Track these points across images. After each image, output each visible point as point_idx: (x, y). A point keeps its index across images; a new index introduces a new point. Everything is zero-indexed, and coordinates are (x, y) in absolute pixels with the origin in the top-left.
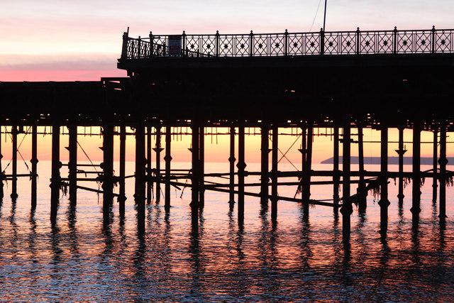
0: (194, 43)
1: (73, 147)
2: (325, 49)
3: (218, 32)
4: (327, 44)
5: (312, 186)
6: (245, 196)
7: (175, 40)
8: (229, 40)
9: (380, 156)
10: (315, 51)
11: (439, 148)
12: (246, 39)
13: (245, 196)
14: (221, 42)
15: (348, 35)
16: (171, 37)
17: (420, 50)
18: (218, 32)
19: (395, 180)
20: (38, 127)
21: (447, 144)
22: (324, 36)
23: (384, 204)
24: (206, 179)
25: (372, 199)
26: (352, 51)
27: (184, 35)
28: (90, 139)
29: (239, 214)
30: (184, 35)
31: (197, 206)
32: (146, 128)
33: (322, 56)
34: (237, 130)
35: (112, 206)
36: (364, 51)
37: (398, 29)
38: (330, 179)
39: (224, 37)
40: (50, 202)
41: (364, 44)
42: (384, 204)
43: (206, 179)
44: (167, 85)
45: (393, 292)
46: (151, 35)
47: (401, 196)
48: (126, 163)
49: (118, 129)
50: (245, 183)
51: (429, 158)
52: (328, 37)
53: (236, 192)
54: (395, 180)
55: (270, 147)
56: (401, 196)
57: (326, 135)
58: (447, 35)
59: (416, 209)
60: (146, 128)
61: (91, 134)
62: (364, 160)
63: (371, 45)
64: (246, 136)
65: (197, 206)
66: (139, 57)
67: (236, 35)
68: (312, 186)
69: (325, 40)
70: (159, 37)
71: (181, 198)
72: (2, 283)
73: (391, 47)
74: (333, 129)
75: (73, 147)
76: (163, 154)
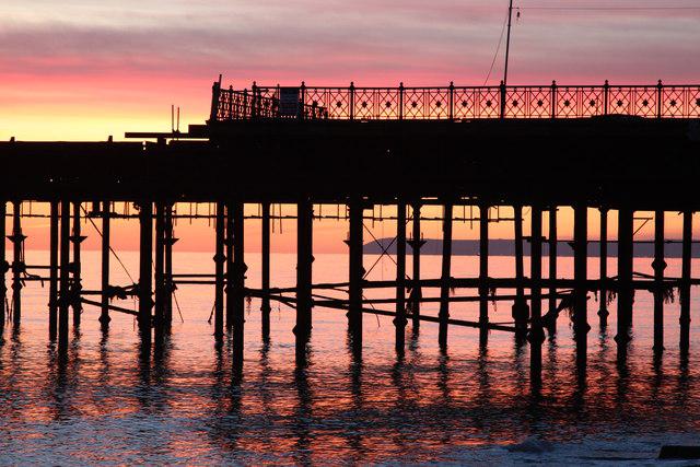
0: (317, 99)
2: (507, 110)
3: (607, 81)
4: (510, 104)
5: (214, 273)
6: (364, 314)
7: (291, 96)
8: (572, 94)
9: (558, 258)
12: (443, 94)
13: (364, 314)
14: (559, 97)
15: (540, 91)
16: (284, 91)
17: (535, 113)
18: (607, 81)
19: (596, 294)
22: (506, 92)
23: (581, 329)
24: (314, 291)
25: (564, 321)
26: (343, 114)
27: (303, 87)
29: (14, 296)
30: (303, 87)
31: (303, 330)
34: (410, 211)
35: (169, 333)
36: (360, 114)
37: (355, 85)
38: (474, 292)
39: (564, 89)
41: (545, 103)
42: (581, 329)
43: (314, 291)
44: (268, 149)
45: (429, 458)
46: (254, 87)
47: (603, 314)
49: (251, 209)
52: (511, 94)
54: (596, 294)
55: (72, 213)
56: (603, 314)
57: (464, 220)
58: (469, 94)
59: (624, 337)
62: (441, 250)
63: (485, 102)
64: (316, 223)
65: (303, 330)
66: (244, 117)
67: (530, 87)
68: (214, 273)
69: (507, 97)
70: (267, 89)
71: (284, 318)
73: (653, 109)
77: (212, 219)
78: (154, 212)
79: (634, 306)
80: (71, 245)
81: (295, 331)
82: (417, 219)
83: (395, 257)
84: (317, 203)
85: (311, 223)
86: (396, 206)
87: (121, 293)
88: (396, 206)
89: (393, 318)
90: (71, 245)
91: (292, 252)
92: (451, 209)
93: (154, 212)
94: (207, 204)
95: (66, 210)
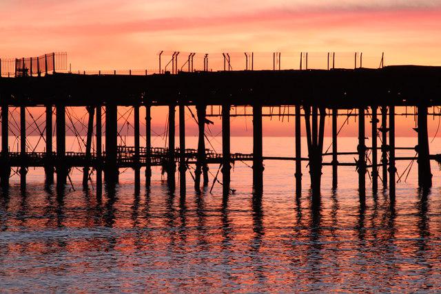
1: (148, 118)
10: (129, 74)
11: (54, 117)
20: (69, 109)
21: (395, 116)
28: (160, 113)
32: (95, 109)
33: (280, 70)
40: (418, 180)
48: (324, 138)
50: (332, 156)
51: (399, 136)
53: (188, 160)
60: (95, 109)
61: (406, 114)
62: (295, 135)
72: (4, 274)
74: (221, 107)
75: (148, 118)
76: (379, 125)
77: (232, 112)
78: (319, 113)
79: (264, 172)
80: (388, 126)
81: (263, 169)
82: (392, 115)
83: (145, 137)
84: (12, 78)
85: (84, 106)
86: (396, 107)
87: (191, 156)
88: (396, 107)
89: (308, 162)
90: (388, 126)
91: (291, 136)
92: (394, 108)
93: (319, 113)
94: (269, 108)
95: (315, 111)
